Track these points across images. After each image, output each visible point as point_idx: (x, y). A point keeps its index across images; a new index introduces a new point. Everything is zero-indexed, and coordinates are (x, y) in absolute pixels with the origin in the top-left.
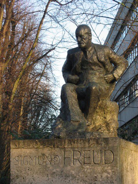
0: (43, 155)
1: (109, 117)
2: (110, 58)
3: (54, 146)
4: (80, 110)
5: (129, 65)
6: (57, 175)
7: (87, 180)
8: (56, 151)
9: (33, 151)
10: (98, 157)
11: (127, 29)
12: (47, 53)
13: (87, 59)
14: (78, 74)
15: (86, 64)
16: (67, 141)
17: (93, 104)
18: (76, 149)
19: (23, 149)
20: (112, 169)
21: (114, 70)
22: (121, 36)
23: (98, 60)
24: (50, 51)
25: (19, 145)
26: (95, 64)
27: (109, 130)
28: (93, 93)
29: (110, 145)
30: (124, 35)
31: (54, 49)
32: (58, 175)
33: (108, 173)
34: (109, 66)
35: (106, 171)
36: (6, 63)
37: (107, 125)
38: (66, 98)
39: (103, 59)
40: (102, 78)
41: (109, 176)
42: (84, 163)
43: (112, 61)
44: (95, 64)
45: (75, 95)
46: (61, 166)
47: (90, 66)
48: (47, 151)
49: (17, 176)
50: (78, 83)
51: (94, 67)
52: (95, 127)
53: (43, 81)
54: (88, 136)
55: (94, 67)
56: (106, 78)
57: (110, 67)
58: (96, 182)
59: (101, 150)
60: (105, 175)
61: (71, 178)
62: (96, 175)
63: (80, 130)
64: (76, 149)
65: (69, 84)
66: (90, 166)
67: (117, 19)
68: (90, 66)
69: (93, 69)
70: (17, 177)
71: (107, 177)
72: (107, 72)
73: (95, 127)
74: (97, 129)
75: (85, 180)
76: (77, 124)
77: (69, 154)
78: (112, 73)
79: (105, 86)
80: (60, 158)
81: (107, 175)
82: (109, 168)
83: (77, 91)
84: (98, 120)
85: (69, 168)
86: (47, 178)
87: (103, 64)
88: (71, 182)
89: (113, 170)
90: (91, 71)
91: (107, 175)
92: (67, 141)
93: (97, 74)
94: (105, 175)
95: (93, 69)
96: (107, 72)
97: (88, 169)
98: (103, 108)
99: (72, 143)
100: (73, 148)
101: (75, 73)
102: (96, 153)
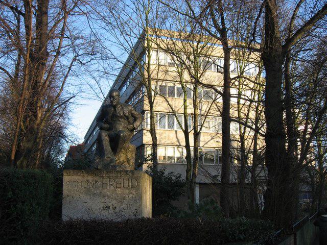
0: (88, 181)
1: (129, 155)
2: (132, 114)
3: (96, 175)
4: (111, 150)
8: (97, 178)
9: (80, 178)
10: (127, 183)
11: (128, 84)
12: (69, 100)
14: (109, 123)
15: (115, 117)
16: (105, 172)
17: (120, 146)
18: (112, 178)
19: (73, 177)
21: (134, 122)
22: (122, 88)
23: (124, 115)
24: (71, 98)
25: (70, 173)
26: (121, 117)
27: (129, 164)
29: (135, 176)
30: (125, 88)
31: (74, 97)
35: (131, 193)
37: (128, 160)
38: (102, 141)
39: (127, 114)
40: (125, 127)
43: (133, 116)
44: (121, 117)
45: (107, 138)
46: (101, 189)
48: (90, 178)
50: (108, 130)
51: (120, 119)
52: (120, 162)
53: (61, 120)
54: (118, 169)
55: (120, 119)
57: (131, 120)
60: (131, 195)
63: (112, 164)
64: (112, 178)
65: (141, 144)
67: (119, 76)
70: (68, 196)
71: (133, 197)
72: (129, 123)
73: (120, 162)
74: (121, 163)
76: (109, 159)
77: (106, 181)
78: (133, 124)
79: (127, 134)
83: (109, 136)
84: (122, 157)
85: (105, 190)
87: (127, 118)
90: (118, 122)
92: (105, 172)
93: (123, 124)
94: (131, 195)
95: (120, 121)
96: (129, 123)
98: (126, 149)
100: (109, 177)
101: (106, 122)
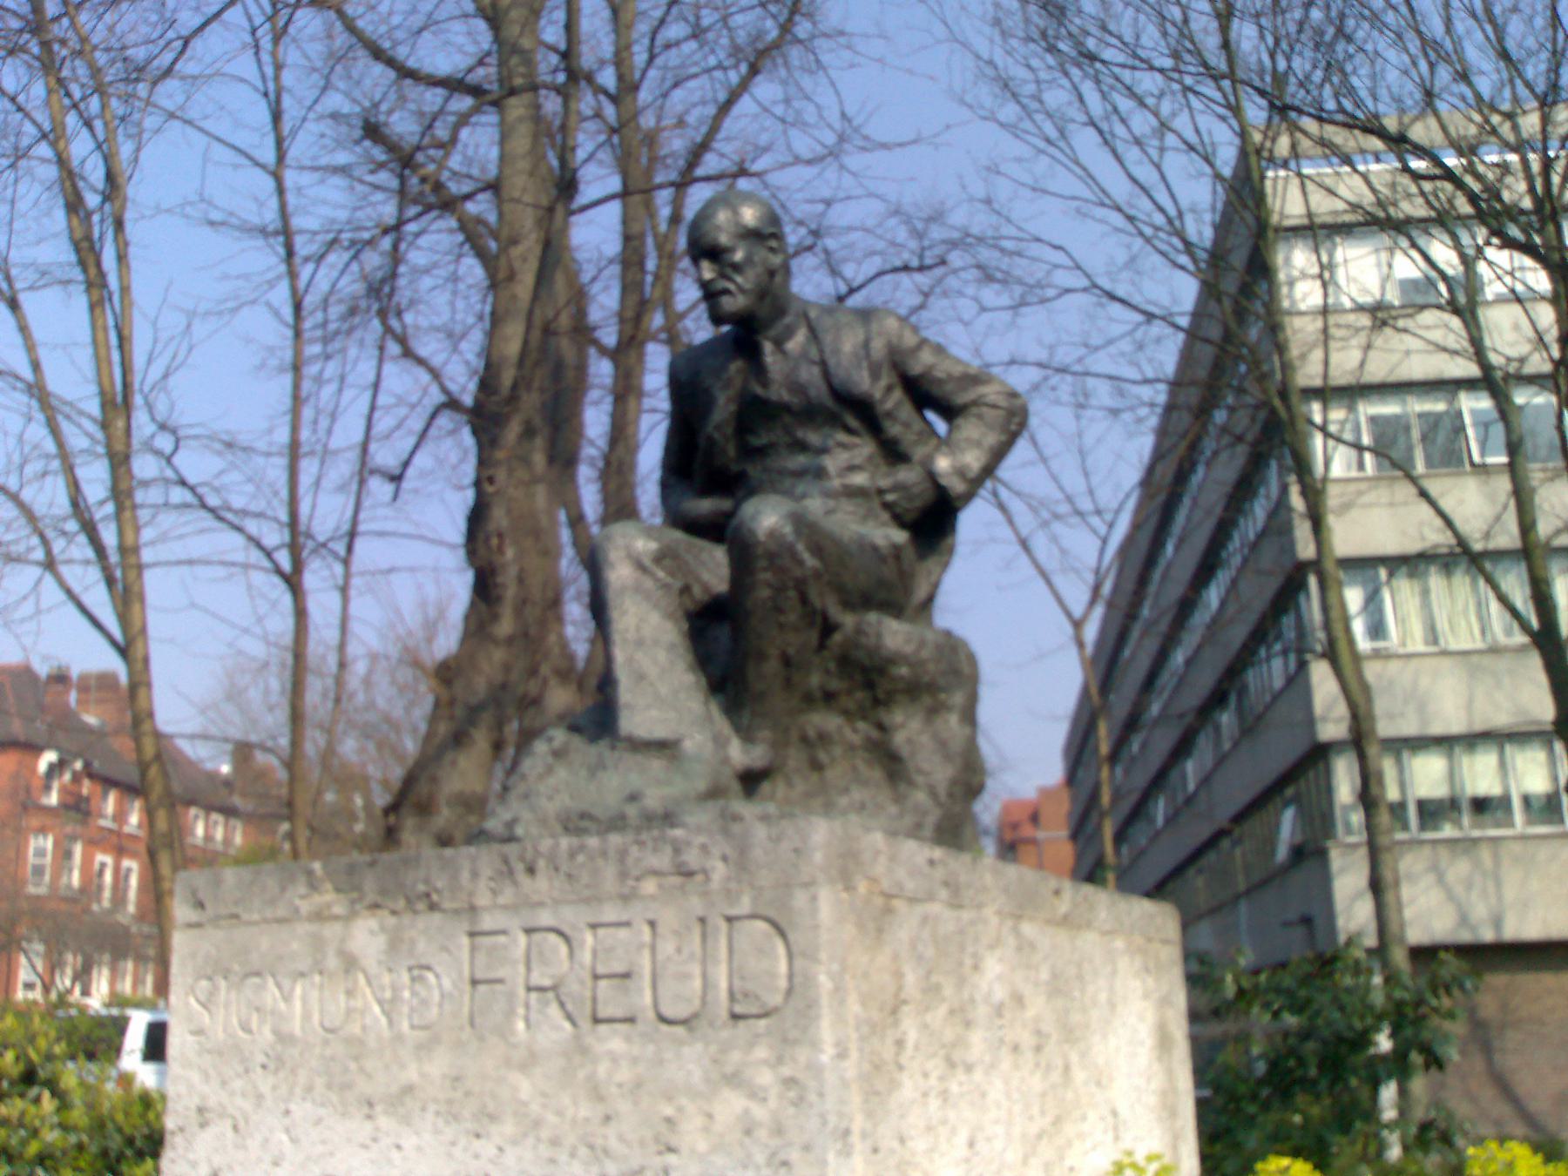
5: (1191, 787)
6: (424, 1109)
7: (613, 1143)
13: (765, 384)
20: (780, 1060)
28: (762, 563)
32: (432, 1108)
33: (756, 1094)
34: (907, 425)
36: (1452, 1054)
41: (759, 1112)
42: (597, 1020)
44: (811, 414)
47: (788, 431)
49: (201, 1110)
56: (890, 497)
58: (671, 1159)
59: (702, 920)
61: (508, 1128)
62: (669, 1111)
66: (628, 1039)
68: (788, 431)
69: (802, 447)
72: (893, 453)
75: (600, 1141)
80: (447, 983)
81: (747, 1112)
82: (761, 1052)
86: (368, 1126)
88: (510, 1157)
89: (786, 1071)
91: (747, 1112)
97: (615, 1059)
99: (522, 877)
102: (667, 947)
